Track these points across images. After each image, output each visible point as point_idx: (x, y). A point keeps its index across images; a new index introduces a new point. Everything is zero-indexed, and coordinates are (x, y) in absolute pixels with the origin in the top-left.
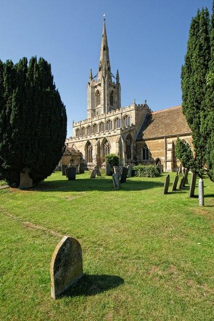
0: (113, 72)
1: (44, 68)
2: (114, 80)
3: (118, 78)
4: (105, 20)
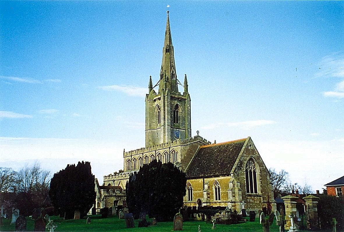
0: (181, 79)
1: (88, 164)
2: (181, 90)
3: (186, 86)
4: (168, 12)
